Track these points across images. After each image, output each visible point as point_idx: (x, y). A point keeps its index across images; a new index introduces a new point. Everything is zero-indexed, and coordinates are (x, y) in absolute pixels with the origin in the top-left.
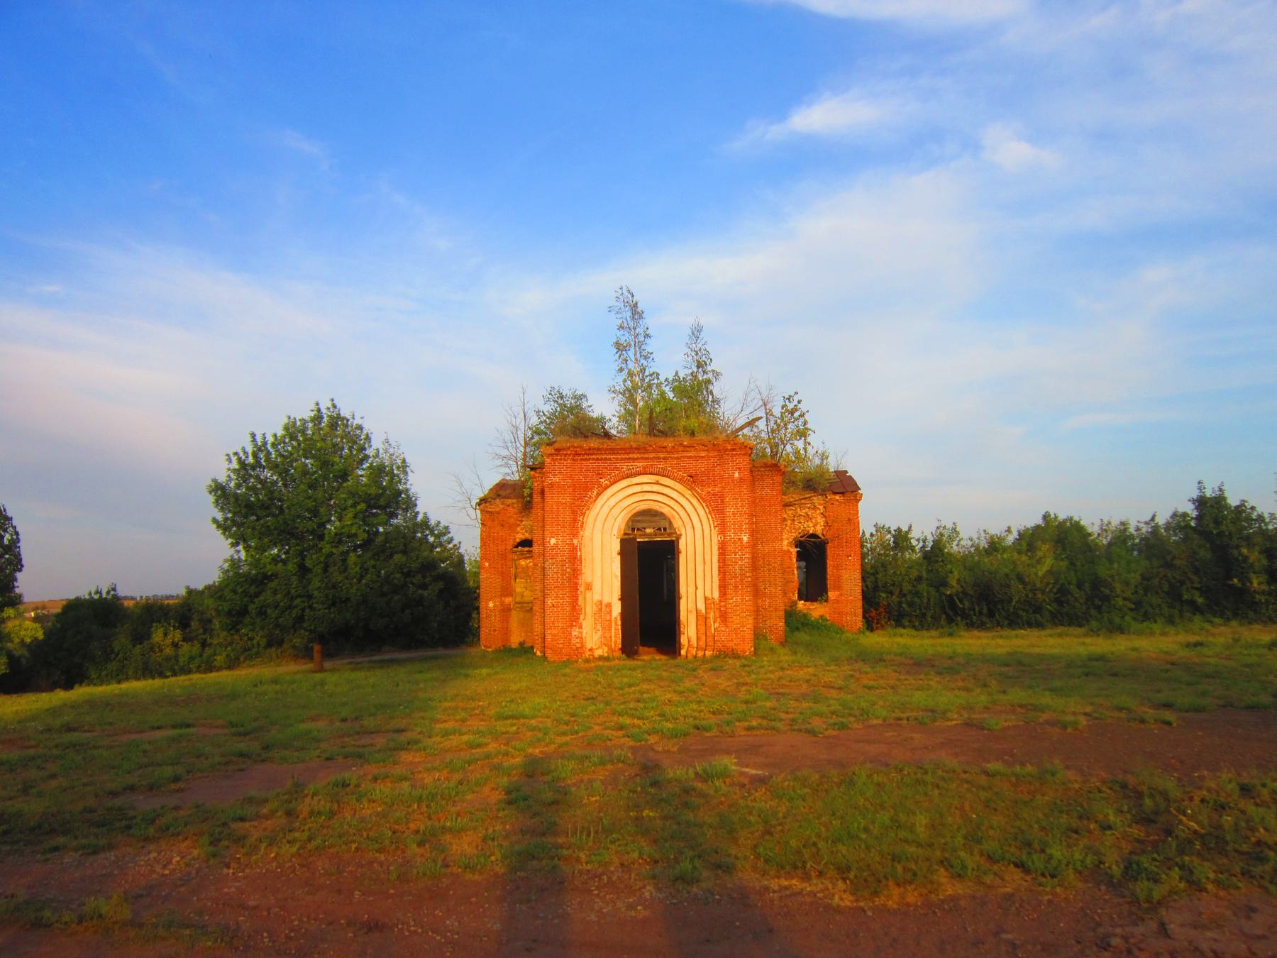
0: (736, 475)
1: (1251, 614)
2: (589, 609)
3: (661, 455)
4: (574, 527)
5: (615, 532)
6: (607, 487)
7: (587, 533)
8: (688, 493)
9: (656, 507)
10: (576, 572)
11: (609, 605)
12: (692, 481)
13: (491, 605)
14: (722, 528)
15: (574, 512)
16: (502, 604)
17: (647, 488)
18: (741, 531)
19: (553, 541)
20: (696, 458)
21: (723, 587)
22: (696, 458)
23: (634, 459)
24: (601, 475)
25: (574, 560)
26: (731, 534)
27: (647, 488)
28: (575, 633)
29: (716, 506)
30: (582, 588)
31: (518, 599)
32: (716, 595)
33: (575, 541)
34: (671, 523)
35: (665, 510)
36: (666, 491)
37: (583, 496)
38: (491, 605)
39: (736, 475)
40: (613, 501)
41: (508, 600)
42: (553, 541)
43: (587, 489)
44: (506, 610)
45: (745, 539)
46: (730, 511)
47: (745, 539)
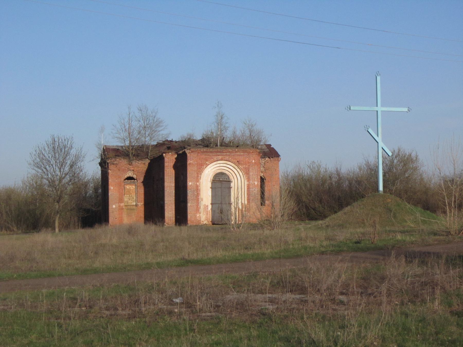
0: (253, 161)
1: (229, 212)
2: (202, 207)
3: (228, 154)
4: (198, 179)
5: (209, 180)
6: (209, 165)
7: (201, 181)
8: (236, 167)
9: (224, 171)
10: (198, 194)
11: (207, 206)
12: (238, 163)
13: (114, 206)
14: (249, 180)
15: (198, 174)
16: (119, 206)
17: (221, 165)
18: (255, 181)
19: (190, 183)
20: (240, 155)
21: (249, 200)
22: (240, 155)
23: (218, 155)
24: (207, 160)
25: (197, 189)
26: (251, 182)
27: (221, 165)
28: (198, 215)
29: (247, 172)
30: (200, 200)
31: (126, 204)
32: (246, 202)
33: (198, 184)
34: (229, 177)
35: (227, 173)
36: (228, 166)
37: (201, 167)
38: (114, 206)
39: (253, 161)
40: (212, 167)
41: (122, 204)
42: (190, 183)
43: (202, 165)
44: (121, 209)
45: (256, 183)
46: (251, 174)
47: (256, 183)
